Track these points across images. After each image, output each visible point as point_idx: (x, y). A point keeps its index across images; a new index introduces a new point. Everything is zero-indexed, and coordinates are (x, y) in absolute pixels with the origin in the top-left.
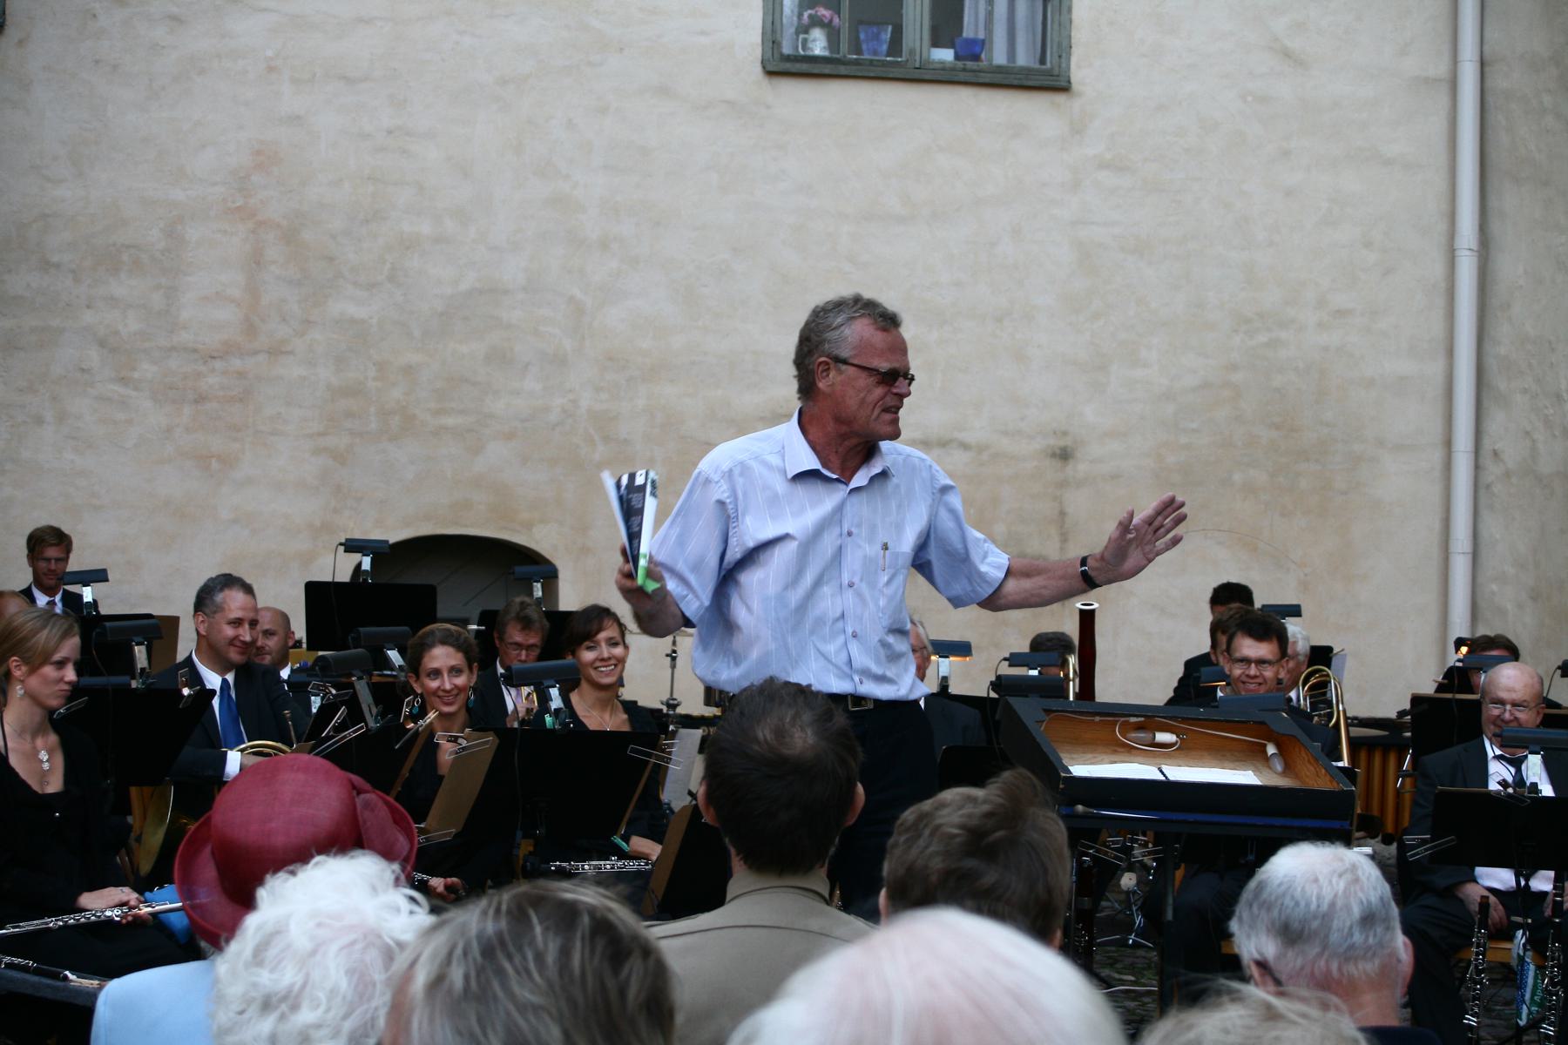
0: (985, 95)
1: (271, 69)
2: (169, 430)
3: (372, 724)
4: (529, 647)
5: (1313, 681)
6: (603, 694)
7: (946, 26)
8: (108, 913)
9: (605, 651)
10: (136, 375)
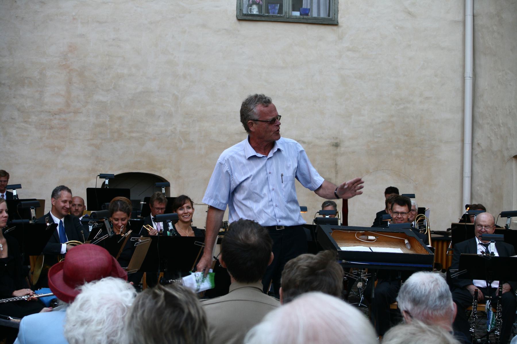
0: (310, 27)
1: (74, 19)
2: (41, 138)
3: (110, 235)
4: (162, 209)
5: (419, 219)
6: (185, 225)
7: (297, 4)
8: (23, 297)
9: (186, 210)
10: (30, 120)
